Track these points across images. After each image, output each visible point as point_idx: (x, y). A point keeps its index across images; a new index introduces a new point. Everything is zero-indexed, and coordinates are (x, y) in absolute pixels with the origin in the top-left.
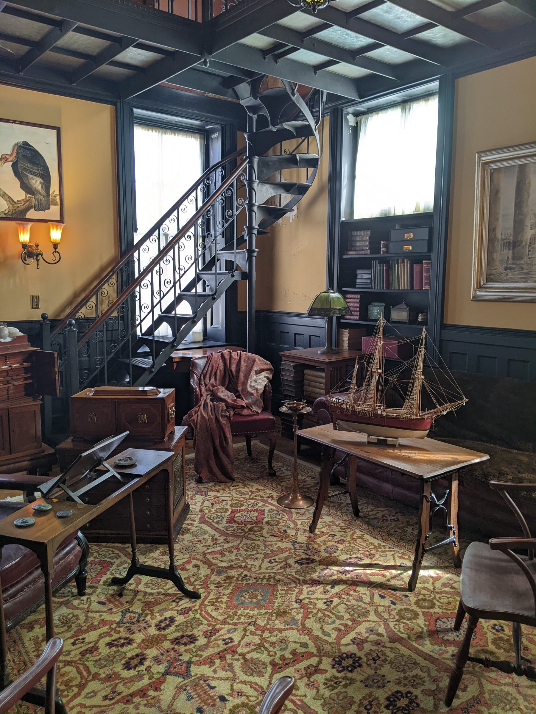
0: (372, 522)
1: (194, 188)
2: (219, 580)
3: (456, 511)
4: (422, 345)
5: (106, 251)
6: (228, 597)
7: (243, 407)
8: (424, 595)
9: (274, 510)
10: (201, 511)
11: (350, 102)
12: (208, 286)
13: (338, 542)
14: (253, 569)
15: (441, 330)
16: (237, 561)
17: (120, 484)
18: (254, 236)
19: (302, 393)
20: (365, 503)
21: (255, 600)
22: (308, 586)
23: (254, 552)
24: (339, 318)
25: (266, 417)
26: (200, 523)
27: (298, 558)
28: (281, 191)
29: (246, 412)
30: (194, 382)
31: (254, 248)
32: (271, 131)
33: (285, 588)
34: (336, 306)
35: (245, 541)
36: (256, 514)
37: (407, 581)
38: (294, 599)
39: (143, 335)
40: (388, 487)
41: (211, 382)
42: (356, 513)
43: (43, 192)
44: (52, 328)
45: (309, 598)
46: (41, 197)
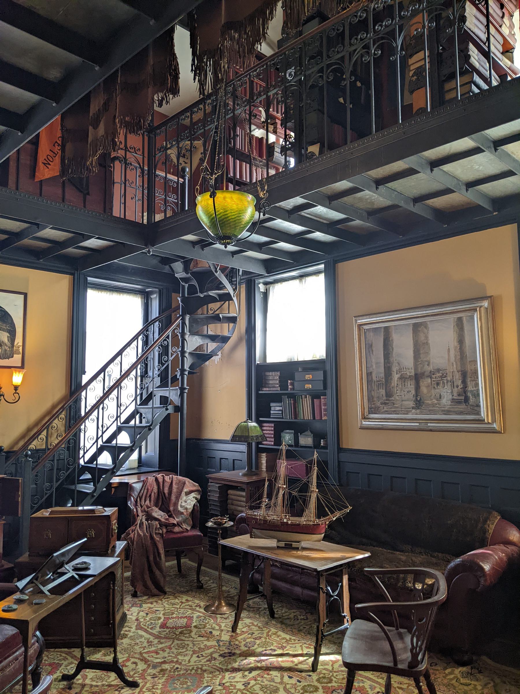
0: (285, 621)
1: (136, 338)
2: (154, 672)
3: (348, 601)
4: (314, 464)
5: (57, 391)
6: (162, 685)
7: (174, 525)
8: (324, 674)
9: (201, 617)
10: (137, 620)
11: (260, 276)
12: (144, 418)
13: (256, 639)
14: (183, 663)
15: (338, 454)
16: (170, 658)
17: (78, 583)
18: (186, 376)
19: (225, 508)
20: (280, 607)
21: (185, 686)
22: (229, 673)
23: (184, 650)
24: (258, 443)
25: (194, 533)
26: (136, 629)
27: (221, 653)
28: (207, 341)
29: (177, 529)
30: (131, 504)
31: (185, 386)
32: (199, 297)
33: (211, 676)
34: (253, 434)
35: (176, 642)
36: (186, 620)
37: (311, 664)
38: (218, 683)
39: (85, 463)
40: (298, 590)
41: (146, 503)
42: (272, 615)
43: (9, 344)
44: (7, 458)
45: (231, 682)
46: (7, 348)
